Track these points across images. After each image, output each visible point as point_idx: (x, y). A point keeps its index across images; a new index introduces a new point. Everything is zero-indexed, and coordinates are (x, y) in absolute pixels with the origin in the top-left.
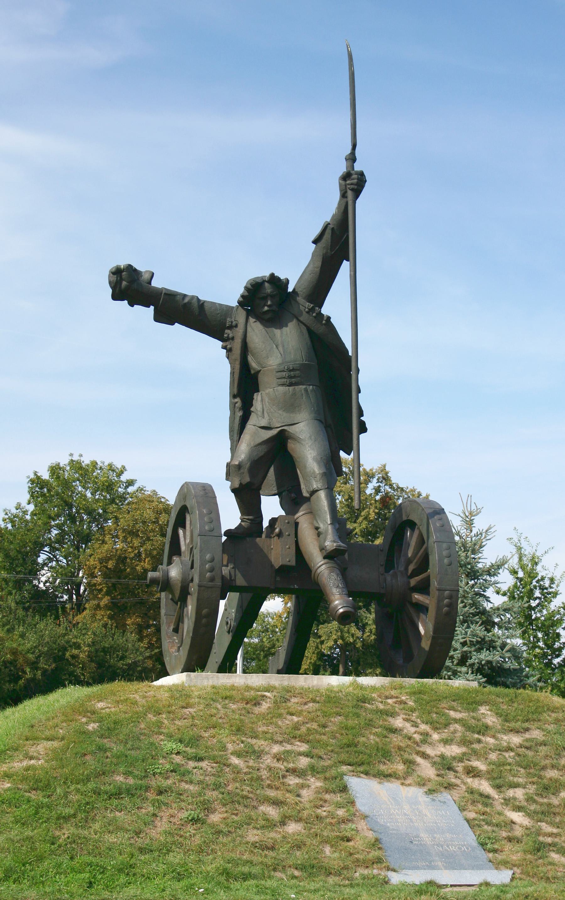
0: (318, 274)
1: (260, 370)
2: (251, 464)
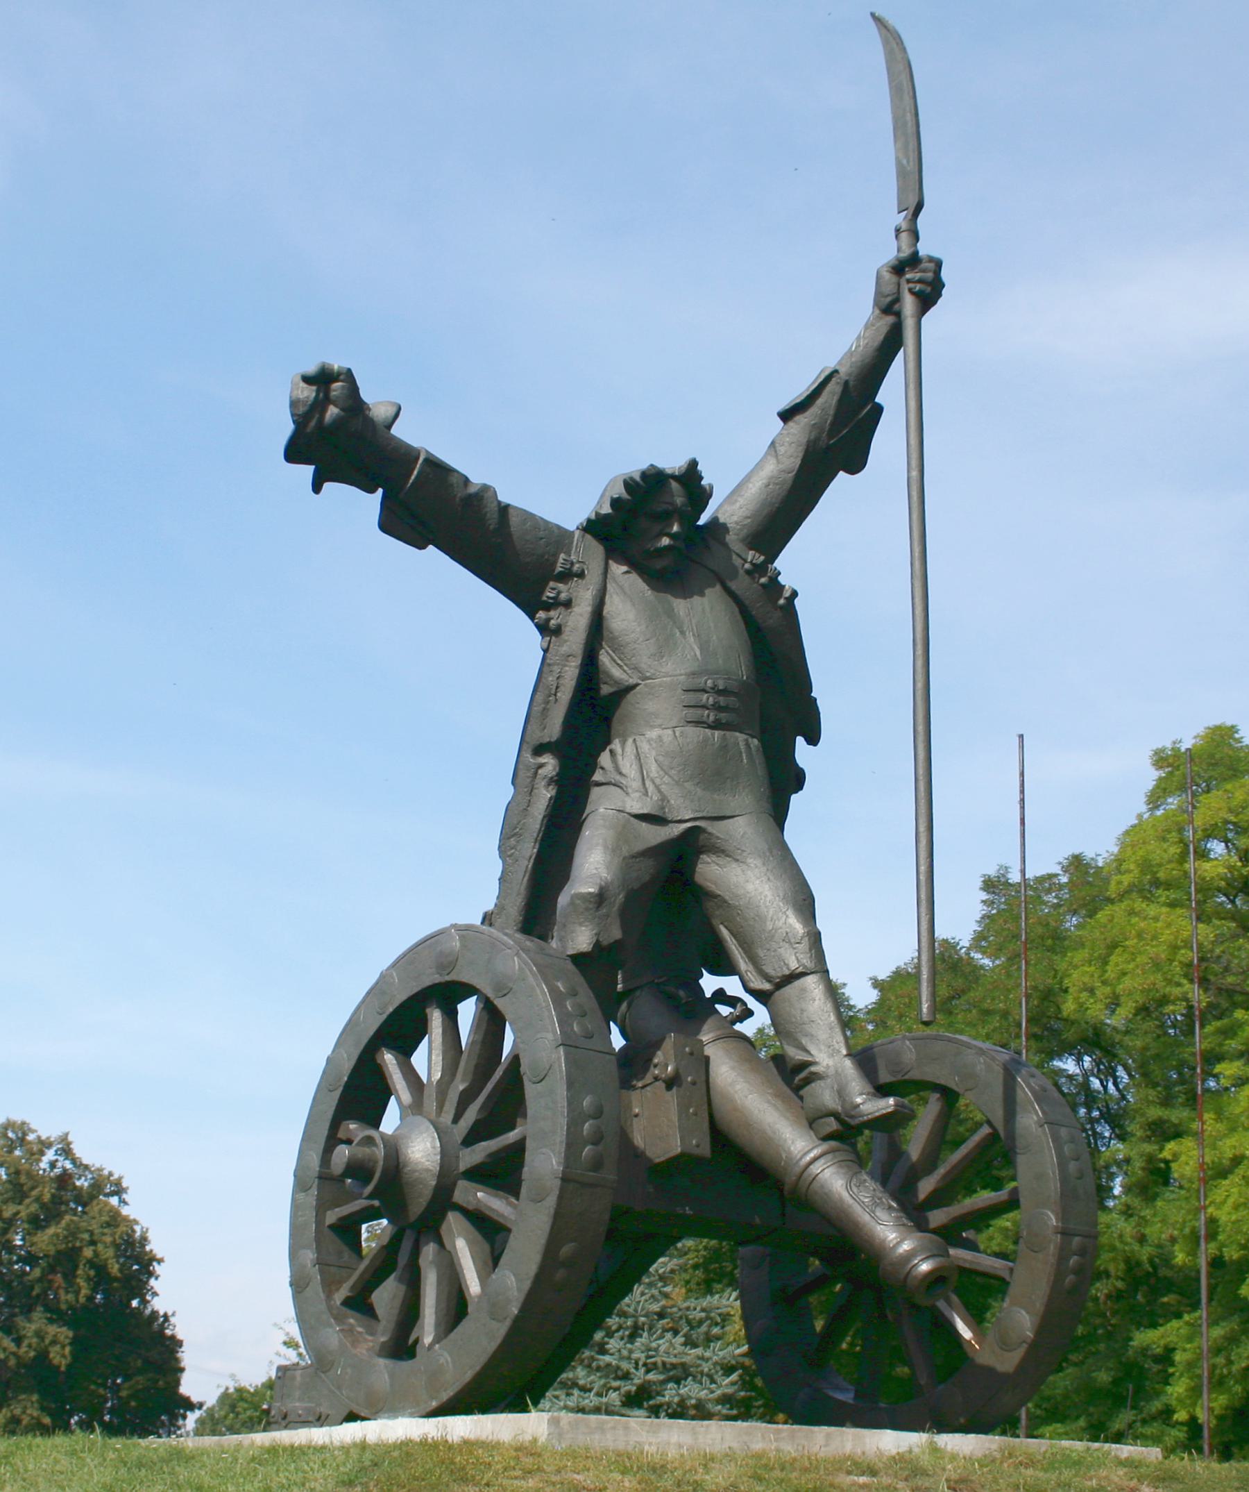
0: (787, 486)
1: (637, 685)
2: (626, 897)
